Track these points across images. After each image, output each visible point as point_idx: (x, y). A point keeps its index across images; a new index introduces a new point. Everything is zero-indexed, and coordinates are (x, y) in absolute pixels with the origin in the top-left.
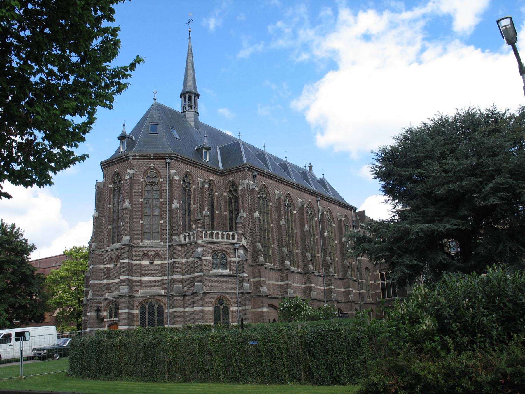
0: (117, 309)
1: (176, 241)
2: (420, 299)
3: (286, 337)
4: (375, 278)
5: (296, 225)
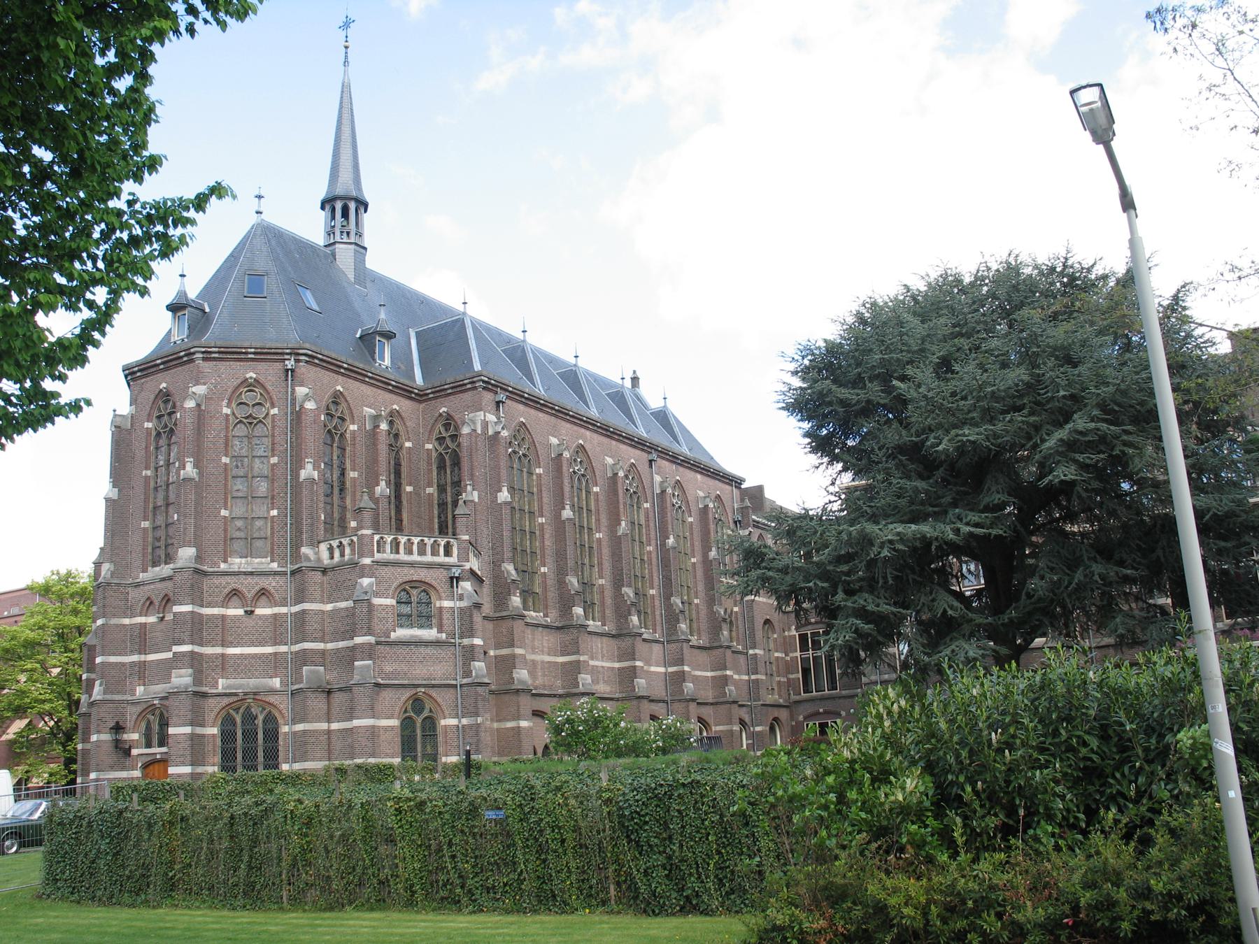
0: (164, 724)
1: (307, 559)
2: (887, 723)
3: (572, 802)
4: (786, 646)
5: (598, 520)
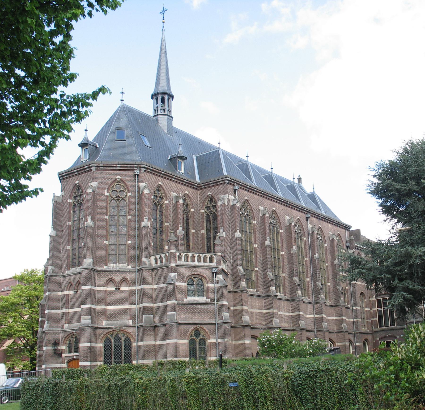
0: (77, 342)
1: (145, 264)
2: (418, 342)
3: (270, 379)
4: (371, 305)
5: (282, 246)
